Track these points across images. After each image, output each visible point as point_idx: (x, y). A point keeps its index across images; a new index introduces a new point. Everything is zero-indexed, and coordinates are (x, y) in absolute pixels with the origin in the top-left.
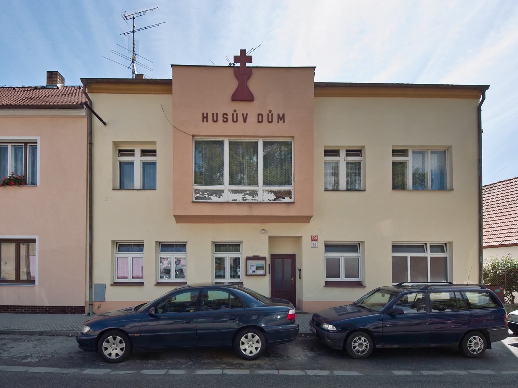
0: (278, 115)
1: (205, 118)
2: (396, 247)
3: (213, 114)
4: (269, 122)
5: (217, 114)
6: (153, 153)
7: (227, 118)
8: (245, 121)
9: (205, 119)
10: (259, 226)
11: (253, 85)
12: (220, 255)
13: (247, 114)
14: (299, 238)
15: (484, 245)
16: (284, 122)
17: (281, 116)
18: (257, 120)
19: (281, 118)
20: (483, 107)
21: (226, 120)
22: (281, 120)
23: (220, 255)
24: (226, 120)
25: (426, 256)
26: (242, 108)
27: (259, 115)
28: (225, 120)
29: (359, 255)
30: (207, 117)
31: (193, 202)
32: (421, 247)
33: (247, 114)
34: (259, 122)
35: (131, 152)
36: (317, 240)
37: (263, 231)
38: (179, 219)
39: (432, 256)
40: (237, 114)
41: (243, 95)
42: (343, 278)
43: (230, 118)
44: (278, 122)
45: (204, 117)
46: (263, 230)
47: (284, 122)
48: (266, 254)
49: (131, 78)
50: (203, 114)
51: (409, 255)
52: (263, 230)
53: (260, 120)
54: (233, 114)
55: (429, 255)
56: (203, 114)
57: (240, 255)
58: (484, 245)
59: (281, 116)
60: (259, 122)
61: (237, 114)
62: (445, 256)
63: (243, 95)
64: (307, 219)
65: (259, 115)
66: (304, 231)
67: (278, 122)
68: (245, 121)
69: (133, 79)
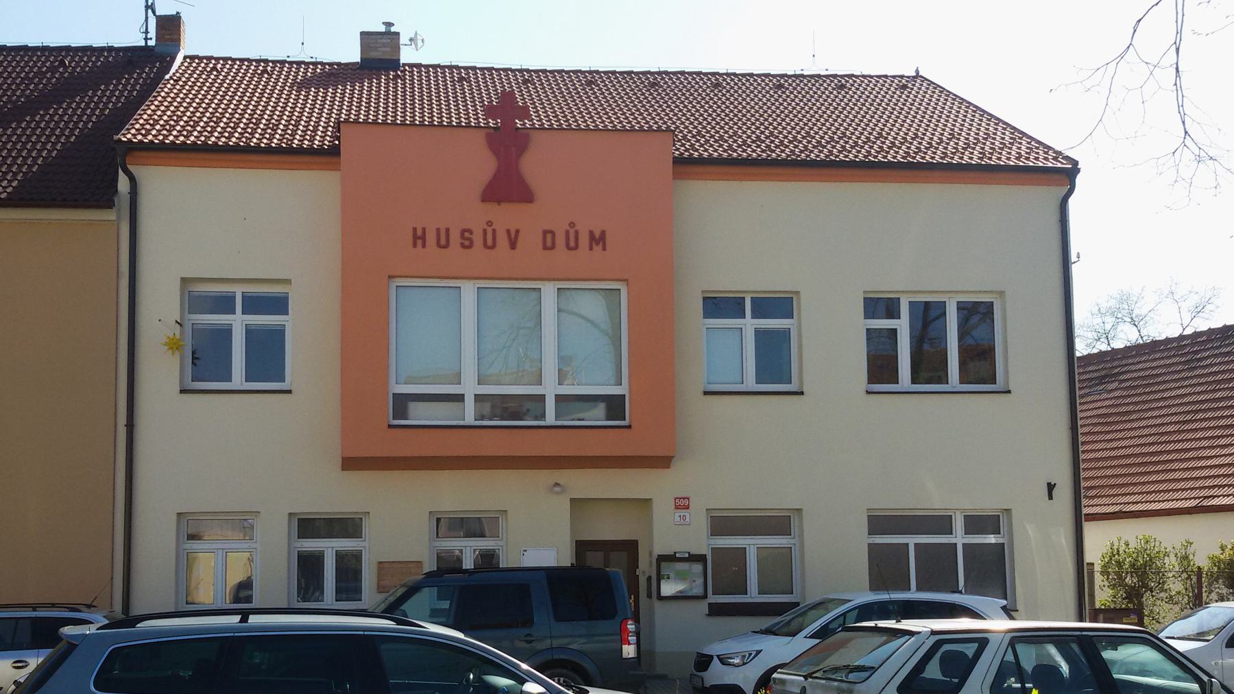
0: (591, 233)
1: (419, 238)
2: (879, 523)
3: (438, 230)
4: (569, 248)
5: (448, 230)
6: (279, 305)
7: (471, 240)
8: (513, 245)
9: (419, 242)
10: (546, 477)
11: (533, 166)
12: (311, 545)
13: (517, 231)
14: (647, 502)
15: (1085, 511)
16: (604, 249)
17: (597, 235)
18: (541, 246)
19: (598, 240)
20: (1071, 200)
21: (467, 244)
22: (597, 244)
23: (311, 545)
24: (466, 234)
25: (953, 541)
26: (506, 216)
27: (545, 232)
28: (467, 243)
29: (792, 541)
30: (423, 238)
31: (390, 426)
32: (942, 524)
33: (517, 231)
34: (545, 248)
35: (224, 304)
36: (687, 507)
37: (557, 489)
38: (350, 463)
39: (966, 541)
40: (494, 231)
41: (507, 187)
42: (753, 595)
43: (477, 238)
44: (591, 249)
45: (415, 237)
46: (557, 484)
47: (604, 249)
48: (704, 550)
49: (142, 43)
50: (415, 229)
51: (912, 540)
52: (557, 484)
53: (549, 243)
54: (485, 231)
55: (959, 538)
56: (415, 229)
57: (712, 542)
58: (1085, 511)
59: (597, 235)
60: (545, 248)
61: (494, 231)
62: (1001, 541)
63: (507, 187)
64: (663, 462)
65: (545, 232)
66: (656, 487)
67: (591, 249)
68: (513, 245)
69: (146, 48)
